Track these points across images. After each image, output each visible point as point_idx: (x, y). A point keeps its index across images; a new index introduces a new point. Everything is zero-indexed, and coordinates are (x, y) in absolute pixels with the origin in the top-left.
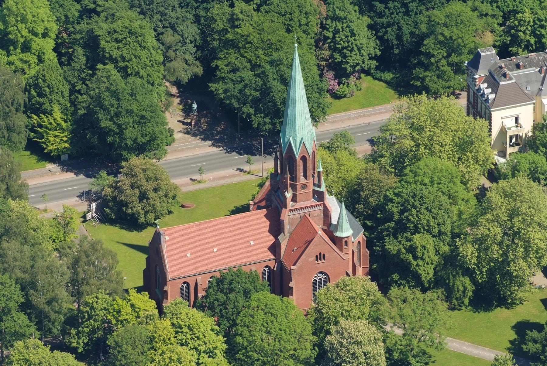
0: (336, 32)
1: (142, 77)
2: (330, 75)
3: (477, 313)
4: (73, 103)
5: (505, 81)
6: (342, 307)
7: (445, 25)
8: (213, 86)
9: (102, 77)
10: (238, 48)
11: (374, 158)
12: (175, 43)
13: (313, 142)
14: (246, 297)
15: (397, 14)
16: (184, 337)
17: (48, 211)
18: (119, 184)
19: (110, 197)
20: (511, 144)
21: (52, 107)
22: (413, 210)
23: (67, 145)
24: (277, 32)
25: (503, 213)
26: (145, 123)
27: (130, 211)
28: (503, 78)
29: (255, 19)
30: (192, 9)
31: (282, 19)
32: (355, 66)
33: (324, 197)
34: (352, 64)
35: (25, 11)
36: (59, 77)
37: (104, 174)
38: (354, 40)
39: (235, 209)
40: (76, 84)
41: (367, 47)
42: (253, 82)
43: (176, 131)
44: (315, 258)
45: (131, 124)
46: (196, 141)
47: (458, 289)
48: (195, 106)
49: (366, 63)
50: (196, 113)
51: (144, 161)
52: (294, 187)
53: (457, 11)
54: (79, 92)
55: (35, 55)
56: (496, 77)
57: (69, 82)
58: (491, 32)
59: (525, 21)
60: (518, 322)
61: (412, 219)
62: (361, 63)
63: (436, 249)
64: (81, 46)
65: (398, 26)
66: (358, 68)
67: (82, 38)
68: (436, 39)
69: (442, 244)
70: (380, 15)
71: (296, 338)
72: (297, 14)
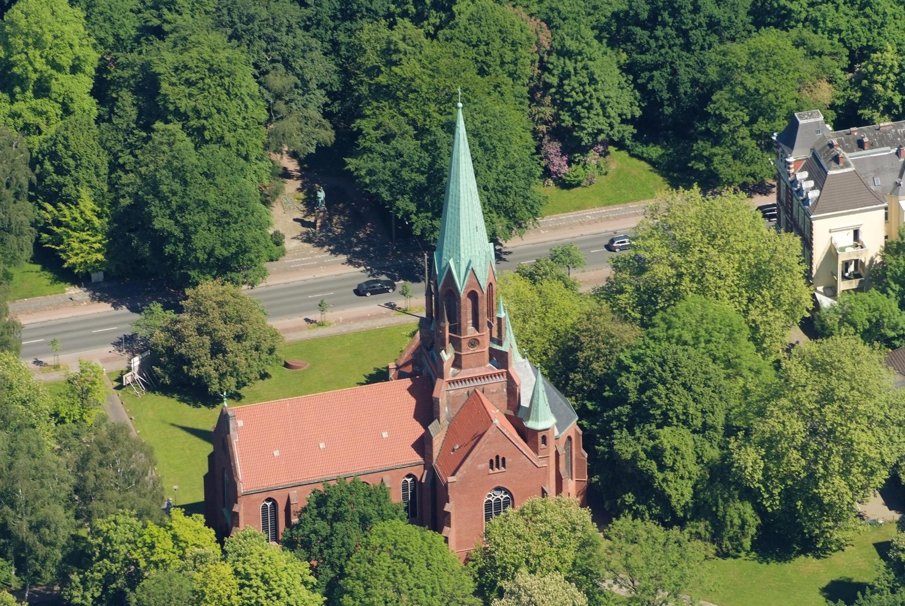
0: (565, 76)
1: (228, 146)
2: (553, 148)
3: (765, 564)
4: (113, 185)
5: (836, 169)
6: (528, 549)
7: (749, 70)
8: (352, 163)
9: (161, 143)
10: (397, 99)
11: (610, 292)
12: (288, 88)
13: (489, 268)
14: (364, 529)
15: (670, 47)
16: (254, 595)
17: (61, 367)
18: (179, 326)
19: (163, 347)
20: (847, 275)
21: (78, 191)
22: (660, 386)
23: (100, 256)
24: (462, 74)
25: (807, 397)
26: (228, 223)
27: (194, 372)
28: (833, 164)
29: (427, 51)
30: (326, 31)
31: (472, 53)
32: (597, 134)
33: (507, 362)
34: (590, 130)
35: (41, 28)
36: (92, 142)
37: (157, 307)
38: (595, 90)
39: (374, 372)
40: (120, 154)
41: (618, 103)
42: (416, 158)
43: (288, 237)
44: (488, 464)
45: (204, 225)
46: (322, 255)
47: (731, 522)
48: (322, 195)
49: (616, 129)
50: (323, 207)
51: (221, 289)
52: (456, 344)
53: (769, 46)
54: (122, 167)
55: (57, 102)
56: (822, 161)
57: (109, 149)
58: (830, 82)
59: (885, 66)
60: (833, 582)
61: (659, 402)
62: (605, 127)
63: (697, 453)
64: (131, 91)
65: (672, 67)
66: (601, 137)
67: (134, 76)
68: (732, 92)
69: (707, 445)
70: (642, 50)
71: (443, 600)
72: (497, 43)
